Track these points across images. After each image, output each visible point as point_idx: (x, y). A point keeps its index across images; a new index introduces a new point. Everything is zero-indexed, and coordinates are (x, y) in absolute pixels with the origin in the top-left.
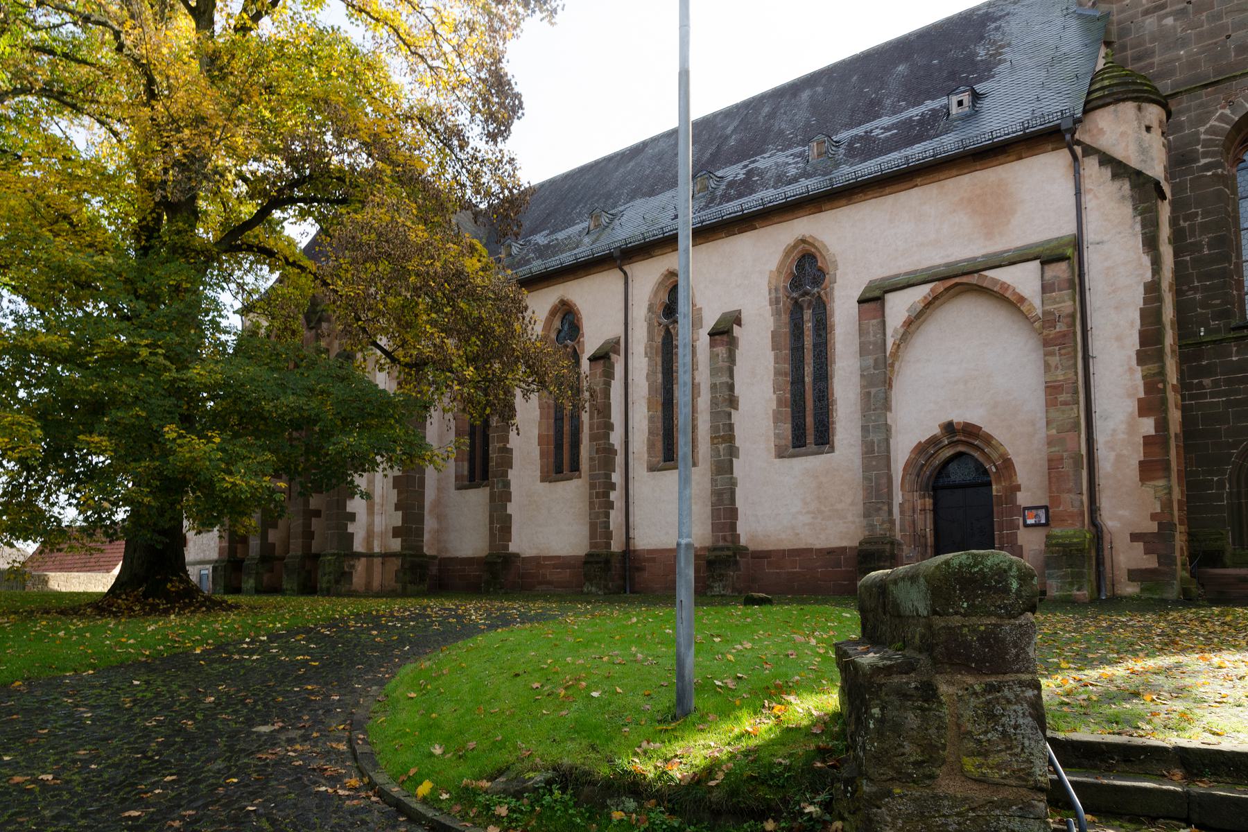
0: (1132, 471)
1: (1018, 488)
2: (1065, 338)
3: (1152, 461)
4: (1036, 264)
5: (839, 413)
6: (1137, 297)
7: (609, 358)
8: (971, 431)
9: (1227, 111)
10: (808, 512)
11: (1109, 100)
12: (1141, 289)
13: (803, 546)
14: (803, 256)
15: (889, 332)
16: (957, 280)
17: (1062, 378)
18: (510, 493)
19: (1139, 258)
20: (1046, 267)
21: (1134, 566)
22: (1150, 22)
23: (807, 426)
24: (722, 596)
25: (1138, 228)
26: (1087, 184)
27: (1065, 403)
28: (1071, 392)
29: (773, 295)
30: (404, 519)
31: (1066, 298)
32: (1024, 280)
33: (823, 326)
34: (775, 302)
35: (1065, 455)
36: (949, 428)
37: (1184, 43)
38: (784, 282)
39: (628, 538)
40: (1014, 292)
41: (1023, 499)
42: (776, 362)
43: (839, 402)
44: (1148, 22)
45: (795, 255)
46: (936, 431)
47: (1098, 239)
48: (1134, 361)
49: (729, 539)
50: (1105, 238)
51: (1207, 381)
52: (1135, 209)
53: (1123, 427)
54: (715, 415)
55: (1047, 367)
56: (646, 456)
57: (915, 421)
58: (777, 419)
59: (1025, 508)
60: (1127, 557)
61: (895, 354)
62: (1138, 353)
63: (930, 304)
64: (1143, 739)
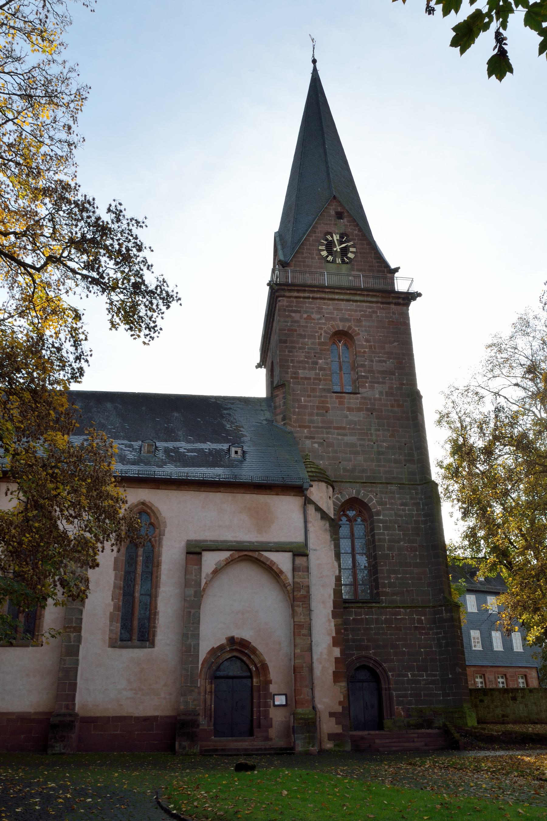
0: (330, 676)
1: (271, 682)
2: (297, 597)
4: (289, 555)
5: (160, 622)
6: (332, 582)
9: (339, 496)
10: (131, 689)
11: (316, 479)
12: (334, 579)
13: (124, 714)
15: (203, 575)
17: (303, 620)
20: (296, 558)
21: (331, 732)
22: (308, 442)
23: (134, 627)
24: (63, 754)
25: (333, 547)
26: (310, 518)
27: (304, 635)
28: (301, 629)
30: (342, 653)
32: (283, 561)
33: (152, 563)
35: (304, 665)
36: (231, 640)
37: (322, 458)
40: (278, 568)
41: (273, 688)
42: (115, 579)
43: (160, 614)
44: (307, 442)
46: (224, 641)
48: (331, 616)
50: (318, 548)
52: (331, 537)
53: (325, 651)
57: (212, 634)
58: (112, 618)
60: (328, 726)
61: (204, 590)
62: (332, 611)
63: (229, 563)
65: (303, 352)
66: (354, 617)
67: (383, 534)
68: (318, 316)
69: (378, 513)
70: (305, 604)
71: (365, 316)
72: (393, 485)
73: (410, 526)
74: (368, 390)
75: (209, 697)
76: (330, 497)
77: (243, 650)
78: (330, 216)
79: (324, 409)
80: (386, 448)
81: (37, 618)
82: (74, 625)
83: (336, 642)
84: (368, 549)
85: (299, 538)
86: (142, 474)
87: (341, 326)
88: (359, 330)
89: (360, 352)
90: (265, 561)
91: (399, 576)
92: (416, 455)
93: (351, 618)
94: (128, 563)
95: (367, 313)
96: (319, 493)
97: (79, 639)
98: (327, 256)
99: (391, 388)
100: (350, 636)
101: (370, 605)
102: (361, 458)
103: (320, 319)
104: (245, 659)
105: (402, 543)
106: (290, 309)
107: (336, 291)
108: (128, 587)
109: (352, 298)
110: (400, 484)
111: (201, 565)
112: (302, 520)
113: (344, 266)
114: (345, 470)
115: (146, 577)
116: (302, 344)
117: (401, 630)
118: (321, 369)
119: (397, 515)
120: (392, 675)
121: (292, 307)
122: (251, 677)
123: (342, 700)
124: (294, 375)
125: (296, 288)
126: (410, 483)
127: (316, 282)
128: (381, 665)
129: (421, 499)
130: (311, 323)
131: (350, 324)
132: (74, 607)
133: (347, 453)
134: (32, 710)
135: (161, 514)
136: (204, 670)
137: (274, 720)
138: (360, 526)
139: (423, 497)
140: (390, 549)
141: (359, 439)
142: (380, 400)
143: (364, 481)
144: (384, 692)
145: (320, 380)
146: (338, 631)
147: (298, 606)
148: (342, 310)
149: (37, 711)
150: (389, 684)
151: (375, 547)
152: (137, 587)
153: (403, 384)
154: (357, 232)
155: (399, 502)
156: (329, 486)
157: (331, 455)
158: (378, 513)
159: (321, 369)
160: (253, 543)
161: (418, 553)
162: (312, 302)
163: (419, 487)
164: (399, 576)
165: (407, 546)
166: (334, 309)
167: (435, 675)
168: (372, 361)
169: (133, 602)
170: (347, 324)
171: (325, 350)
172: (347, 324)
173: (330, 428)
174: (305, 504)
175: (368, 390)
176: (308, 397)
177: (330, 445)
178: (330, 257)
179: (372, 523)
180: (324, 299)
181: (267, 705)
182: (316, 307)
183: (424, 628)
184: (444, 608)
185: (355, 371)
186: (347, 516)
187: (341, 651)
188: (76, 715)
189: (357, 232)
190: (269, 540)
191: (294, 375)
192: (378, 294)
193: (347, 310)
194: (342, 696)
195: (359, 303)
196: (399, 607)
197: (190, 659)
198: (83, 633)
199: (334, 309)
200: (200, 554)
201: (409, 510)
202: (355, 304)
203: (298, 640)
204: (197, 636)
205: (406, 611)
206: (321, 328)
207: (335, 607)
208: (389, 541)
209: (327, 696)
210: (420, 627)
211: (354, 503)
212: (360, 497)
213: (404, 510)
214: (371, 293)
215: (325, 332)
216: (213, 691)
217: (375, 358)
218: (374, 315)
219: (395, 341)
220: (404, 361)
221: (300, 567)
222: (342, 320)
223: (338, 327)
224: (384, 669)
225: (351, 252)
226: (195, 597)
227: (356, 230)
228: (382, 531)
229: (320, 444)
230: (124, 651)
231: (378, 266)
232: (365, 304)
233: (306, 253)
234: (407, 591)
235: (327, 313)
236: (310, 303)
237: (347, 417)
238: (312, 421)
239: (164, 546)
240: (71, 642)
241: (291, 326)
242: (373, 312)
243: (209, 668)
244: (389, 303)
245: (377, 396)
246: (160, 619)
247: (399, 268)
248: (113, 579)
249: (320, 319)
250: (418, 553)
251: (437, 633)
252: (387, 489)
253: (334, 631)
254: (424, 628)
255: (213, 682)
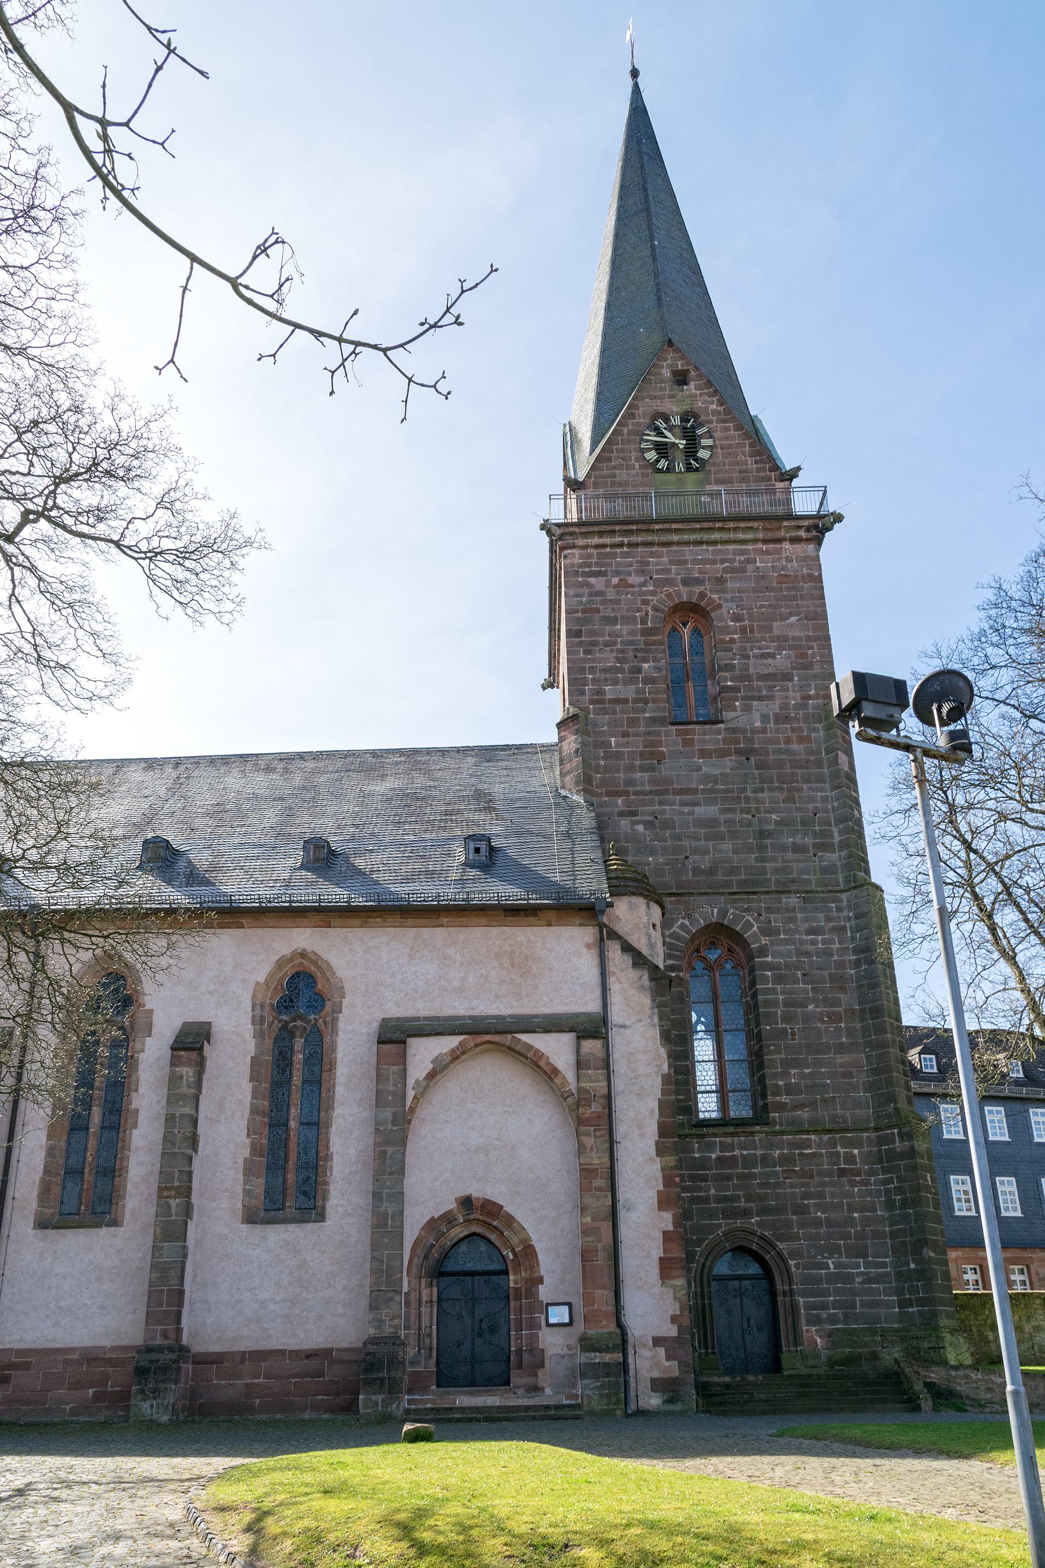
1: (540, 1280)
2: (591, 1116)
3: (671, 1259)
4: (573, 1035)
5: (335, 1173)
8: (491, 1210)
9: (687, 922)
14: (298, 974)
15: (410, 1082)
16: (489, 1037)
17: (596, 1161)
19: (658, 1050)
21: (656, 1374)
22: (624, 823)
23: (288, 1184)
25: (656, 1020)
26: (611, 967)
28: (599, 1181)
29: (258, 1012)
31: (601, 1078)
33: (320, 1061)
34: (258, 1021)
36: (466, 1202)
38: (271, 999)
40: (549, 1063)
41: (544, 1293)
43: (336, 1159)
44: (623, 822)
45: (289, 970)
46: (451, 1205)
47: (621, 1022)
48: (653, 1152)
49: (172, 1335)
50: (627, 1023)
52: (653, 1001)
54: (168, 1155)
55: (581, 1149)
56: (34, 1205)
57: (430, 1191)
58: (249, 1169)
59: (548, 1305)
60: (648, 1364)
61: (412, 1110)
62: (657, 1143)
63: (456, 1055)
65: (612, 651)
66: (719, 1153)
67: (774, 991)
68: (640, 580)
69: (763, 951)
70: (599, 1130)
71: (733, 570)
72: (792, 895)
73: (826, 973)
74: (739, 713)
75: (428, 1310)
76: (654, 926)
77: (489, 1220)
78: (662, 382)
79: (653, 756)
80: (777, 823)
81: (117, 1174)
82: (177, 1184)
83: (664, 1202)
84: (748, 1022)
85: (592, 1006)
86: (297, 902)
87: (685, 594)
88: (720, 598)
89: (722, 641)
90: (523, 1051)
91: (807, 1071)
92: (836, 835)
93: (714, 1156)
94: (278, 1067)
95: (736, 564)
96: (635, 917)
97: (188, 1210)
98: (658, 461)
99: (785, 706)
100: (713, 1191)
101: (750, 1129)
102: (727, 846)
103: (644, 584)
104: (493, 1237)
105: (811, 1007)
106: (587, 570)
107: (674, 526)
108: (278, 1111)
109: (705, 536)
110: (807, 892)
111: (405, 1063)
112: (596, 971)
113: (692, 476)
114: (697, 871)
115: (311, 1091)
116: (610, 635)
117: (812, 1177)
118: (647, 681)
119: (800, 953)
120: (797, 1266)
121: (590, 565)
122: (506, 1272)
123: (678, 1313)
124: (595, 697)
125: (596, 529)
126: (824, 889)
127: (635, 514)
128: (774, 1247)
129: (849, 919)
130: (628, 593)
131: (702, 588)
132: (176, 1150)
133: (699, 839)
134: (107, 1344)
135: (334, 973)
136: (416, 1260)
137: (550, 1352)
138: (729, 978)
139: (851, 914)
140: (788, 1018)
141: (723, 811)
142: (764, 730)
143: (735, 890)
144: (780, 1299)
145: (646, 701)
146: (668, 1181)
147: (588, 1134)
148: (686, 562)
149: (117, 1344)
150: (790, 1283)
151: (758, 1015)
152: (293, 1110)
153: (809, 697)
154: (714, 407)
155: (805, 926)
156: (651, 903)
157: (669, 843)
158: (763, 951)
159: (647, 681)
160: (504, 1018)
161: (843, 1025)
162: (628, 553)
163: (844, 896)
164: (807, 1071)
165: (821, 1013)
166: (671, 562)
167: (884, 1265)
168: (747, 657)
169: (287, 1138)
170: (697, 590)
171: (654, 643)
172: (697, 590)
173: (665, 792)
174: (602, 940)
175: (739, 713)
176: (623, 736)
177: (667, 825)
178: (663, 461)
179: (752, 970)
180: (651, 544)
181: (534, 1325)
182: (636, 562)
183: (858, 1173)
184: (896, 1131)
185: (714, 679)
186: (704, 959)
187: (674, 1219)
188: (183, 1350)
189: (714, 407)
190: (534, 1012)
191: (595, 697)
192: (755, 524)
193: (696, 562)
194: (677, 1306)
195: (719, 547)
196: (808, 1132)
197: (386, 1240)
198: (195, 1198)
199: (671, 562)
200: (405, 1043)
201: (824, 942)
202: (711, 549)
203: (589, 1201)
204: (399, 1197)
205: (821, 1139)
206: (646, 602)
207: (661, 1134)
208: (787, 1004)
209: (652, 1308)
210: (850, 1170)
211: (720, 933)
212: (726, 922)
213: (814, 943)
214: (742, 525)
215: (655, 609)
216: (435, 1299)
217: (752, 650)
218: (750, 567)
219: (791, 614)
220: (810, 652)
221: (589, 1061)
222: (686, 582)
223: (680, 596)
224: (779, 1254)
225: (703, 447)
226: (393, 1123)
227: (713, 403)
228: (770, 985)
229: (649, 825)
230: (270, 1228)
231: (758, 470)
232: (731, 547)
233: (617, 458)
234: (824, 1100)
235: (658, 572)
236: (624, 555)
237: (699, 769)
238: (631, 782)
239: (340, 1033)
240: (171, 1215)
241: (589, 602)
242: (748, 561)
243: (426, 1257)
244: (779, 541)
245: (758, 724)
246: (334, 1166)
247: (799, 469)
248: (249, 1098)
249: (644, 584)
250: (843, 1025)
251: (886, 1182)
252: (780, 902)
253: (661, 1181)
254: (858, 1173)
255: (435, 1283)
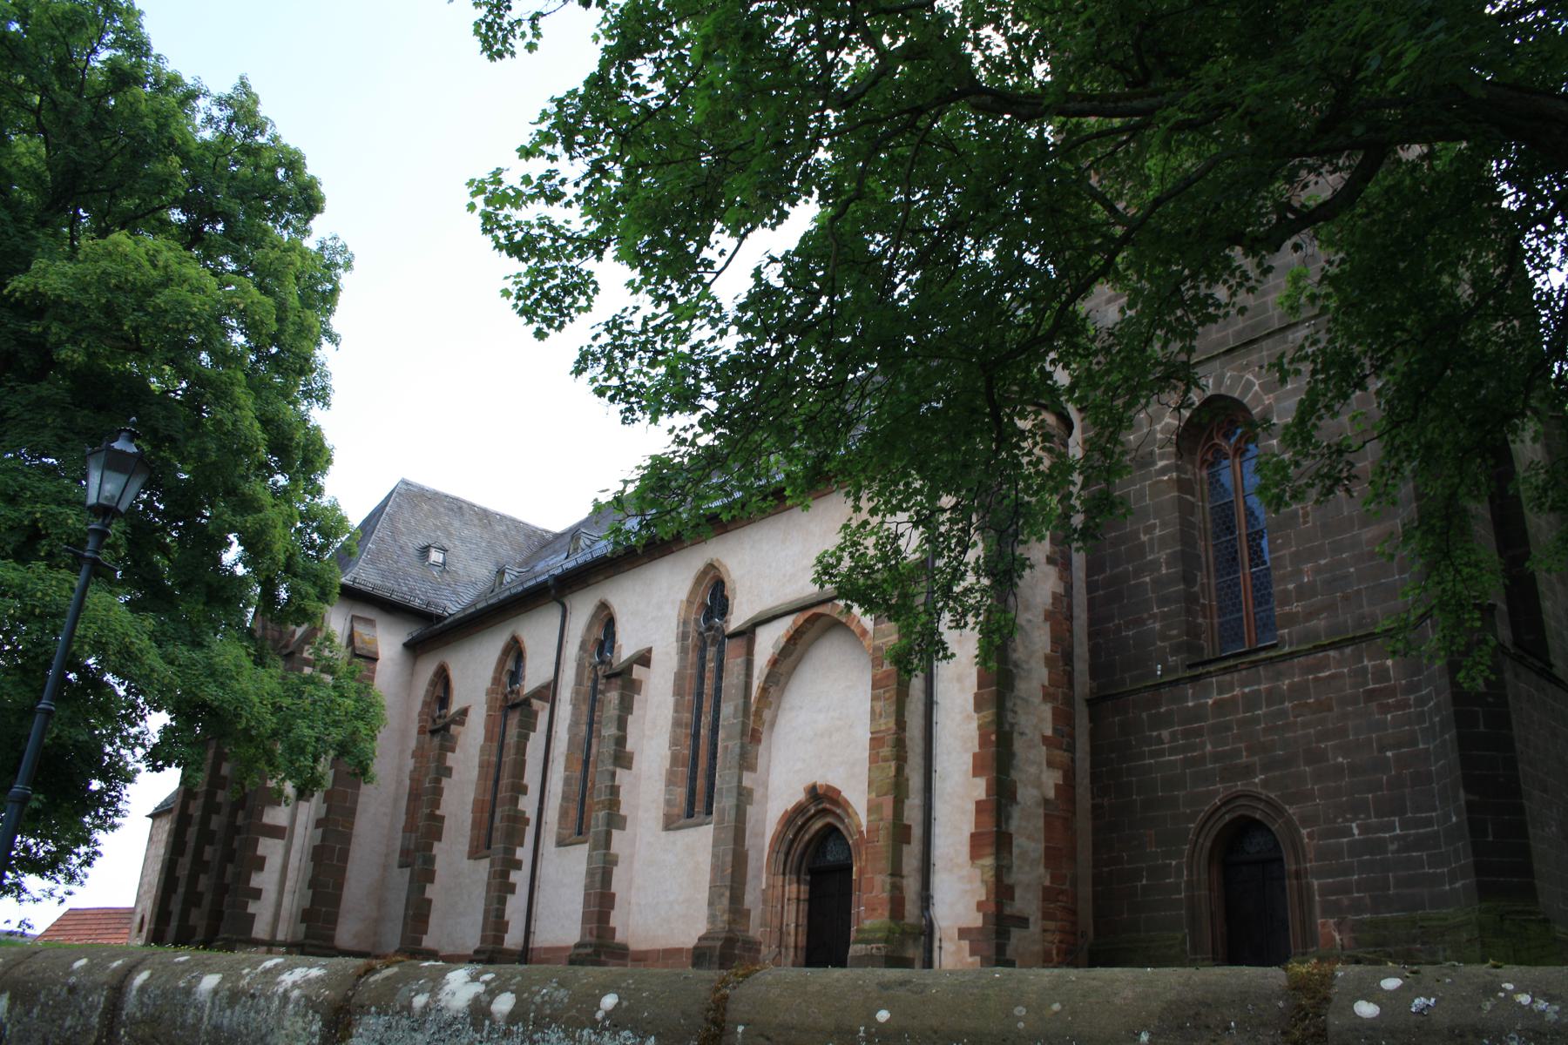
7: (530, 705)
18: (433, 872)
23: (699, 792)
34: (683, 637)
39: (528, 932)
51: (1165, 734)
58: (671, 781)
62: (976, 696)
64: (147, 919)
